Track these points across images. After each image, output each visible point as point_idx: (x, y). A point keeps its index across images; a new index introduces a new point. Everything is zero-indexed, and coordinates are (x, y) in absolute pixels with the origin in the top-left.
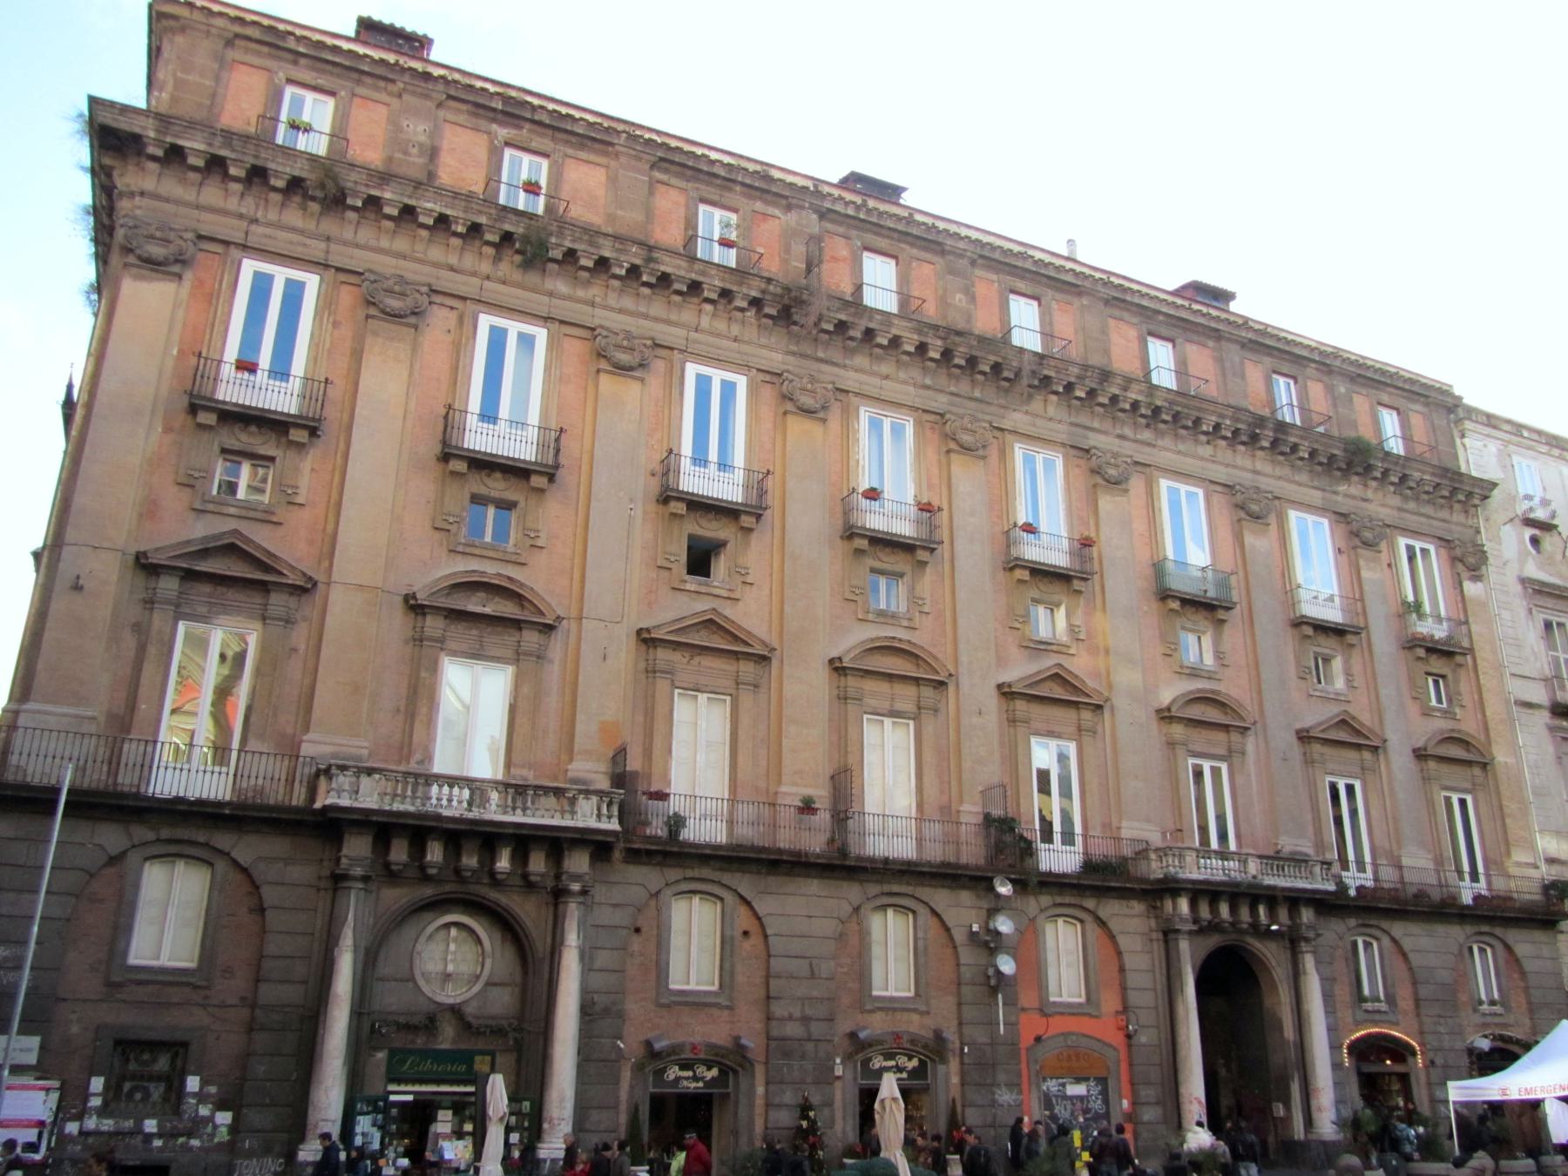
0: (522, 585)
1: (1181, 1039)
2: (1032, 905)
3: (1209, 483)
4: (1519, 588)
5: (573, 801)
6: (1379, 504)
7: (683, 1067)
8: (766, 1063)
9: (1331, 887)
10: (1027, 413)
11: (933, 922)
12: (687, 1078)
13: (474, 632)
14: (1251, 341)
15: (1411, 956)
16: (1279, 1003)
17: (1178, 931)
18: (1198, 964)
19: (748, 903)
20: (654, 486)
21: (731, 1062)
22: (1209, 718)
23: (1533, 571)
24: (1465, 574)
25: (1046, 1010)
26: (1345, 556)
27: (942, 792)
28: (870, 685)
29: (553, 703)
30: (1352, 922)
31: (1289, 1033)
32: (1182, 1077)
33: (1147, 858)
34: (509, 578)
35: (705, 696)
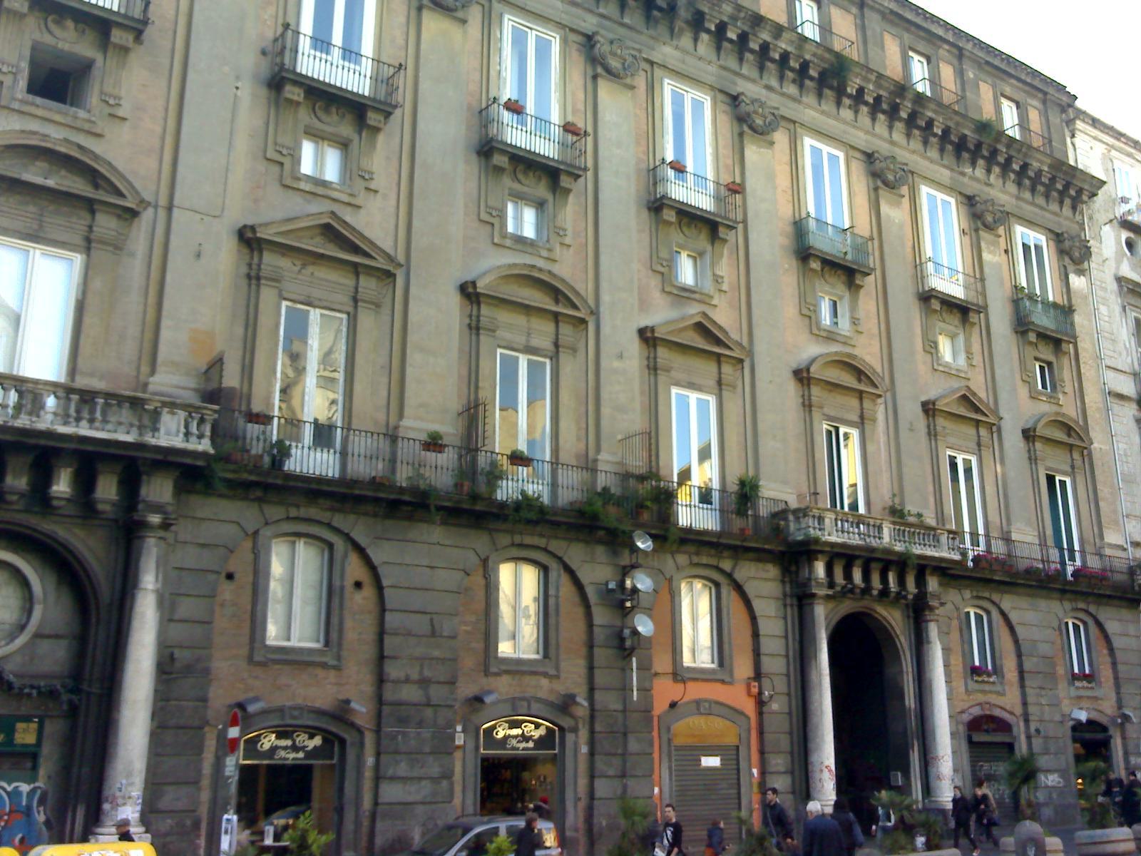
0: (96, 157)
1: (813, 706)
2: (668, 563)
3: (850, 147)
4: (1115, 286)
5: (156, 415)
6: (1001, 192)
7: (280, 735)
8: (378, 731)
9: (957, 557)
10: (677, 48)
11: (565, 580)
12: (285, 748)
13: (31, 208)
14: (892, 12)
15: (1019, 629)
16: (901, 672)
17: (814, 595)
18: (831, 627)
19: (361, 551)
20: (265, 68)
21: (335, 729)
22: (840, 385)
23: (1126, 271)
24: (1071, 268)
25: (679, 675)
26: (967, 237)
27: (578, 439)
28: (504, 317)
29: (132, 305)
30: (967, 594)
31: (910, 701)
32: (811, 745)
33: (786, 519)
34: (80, 147)
35: (318, 311)
